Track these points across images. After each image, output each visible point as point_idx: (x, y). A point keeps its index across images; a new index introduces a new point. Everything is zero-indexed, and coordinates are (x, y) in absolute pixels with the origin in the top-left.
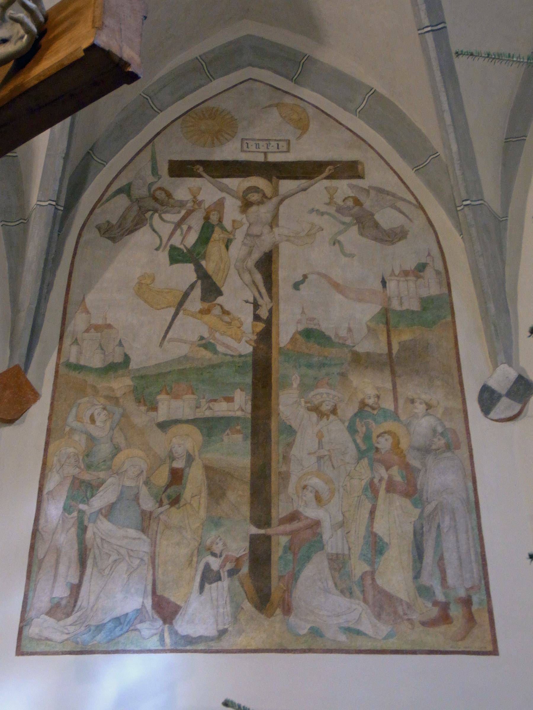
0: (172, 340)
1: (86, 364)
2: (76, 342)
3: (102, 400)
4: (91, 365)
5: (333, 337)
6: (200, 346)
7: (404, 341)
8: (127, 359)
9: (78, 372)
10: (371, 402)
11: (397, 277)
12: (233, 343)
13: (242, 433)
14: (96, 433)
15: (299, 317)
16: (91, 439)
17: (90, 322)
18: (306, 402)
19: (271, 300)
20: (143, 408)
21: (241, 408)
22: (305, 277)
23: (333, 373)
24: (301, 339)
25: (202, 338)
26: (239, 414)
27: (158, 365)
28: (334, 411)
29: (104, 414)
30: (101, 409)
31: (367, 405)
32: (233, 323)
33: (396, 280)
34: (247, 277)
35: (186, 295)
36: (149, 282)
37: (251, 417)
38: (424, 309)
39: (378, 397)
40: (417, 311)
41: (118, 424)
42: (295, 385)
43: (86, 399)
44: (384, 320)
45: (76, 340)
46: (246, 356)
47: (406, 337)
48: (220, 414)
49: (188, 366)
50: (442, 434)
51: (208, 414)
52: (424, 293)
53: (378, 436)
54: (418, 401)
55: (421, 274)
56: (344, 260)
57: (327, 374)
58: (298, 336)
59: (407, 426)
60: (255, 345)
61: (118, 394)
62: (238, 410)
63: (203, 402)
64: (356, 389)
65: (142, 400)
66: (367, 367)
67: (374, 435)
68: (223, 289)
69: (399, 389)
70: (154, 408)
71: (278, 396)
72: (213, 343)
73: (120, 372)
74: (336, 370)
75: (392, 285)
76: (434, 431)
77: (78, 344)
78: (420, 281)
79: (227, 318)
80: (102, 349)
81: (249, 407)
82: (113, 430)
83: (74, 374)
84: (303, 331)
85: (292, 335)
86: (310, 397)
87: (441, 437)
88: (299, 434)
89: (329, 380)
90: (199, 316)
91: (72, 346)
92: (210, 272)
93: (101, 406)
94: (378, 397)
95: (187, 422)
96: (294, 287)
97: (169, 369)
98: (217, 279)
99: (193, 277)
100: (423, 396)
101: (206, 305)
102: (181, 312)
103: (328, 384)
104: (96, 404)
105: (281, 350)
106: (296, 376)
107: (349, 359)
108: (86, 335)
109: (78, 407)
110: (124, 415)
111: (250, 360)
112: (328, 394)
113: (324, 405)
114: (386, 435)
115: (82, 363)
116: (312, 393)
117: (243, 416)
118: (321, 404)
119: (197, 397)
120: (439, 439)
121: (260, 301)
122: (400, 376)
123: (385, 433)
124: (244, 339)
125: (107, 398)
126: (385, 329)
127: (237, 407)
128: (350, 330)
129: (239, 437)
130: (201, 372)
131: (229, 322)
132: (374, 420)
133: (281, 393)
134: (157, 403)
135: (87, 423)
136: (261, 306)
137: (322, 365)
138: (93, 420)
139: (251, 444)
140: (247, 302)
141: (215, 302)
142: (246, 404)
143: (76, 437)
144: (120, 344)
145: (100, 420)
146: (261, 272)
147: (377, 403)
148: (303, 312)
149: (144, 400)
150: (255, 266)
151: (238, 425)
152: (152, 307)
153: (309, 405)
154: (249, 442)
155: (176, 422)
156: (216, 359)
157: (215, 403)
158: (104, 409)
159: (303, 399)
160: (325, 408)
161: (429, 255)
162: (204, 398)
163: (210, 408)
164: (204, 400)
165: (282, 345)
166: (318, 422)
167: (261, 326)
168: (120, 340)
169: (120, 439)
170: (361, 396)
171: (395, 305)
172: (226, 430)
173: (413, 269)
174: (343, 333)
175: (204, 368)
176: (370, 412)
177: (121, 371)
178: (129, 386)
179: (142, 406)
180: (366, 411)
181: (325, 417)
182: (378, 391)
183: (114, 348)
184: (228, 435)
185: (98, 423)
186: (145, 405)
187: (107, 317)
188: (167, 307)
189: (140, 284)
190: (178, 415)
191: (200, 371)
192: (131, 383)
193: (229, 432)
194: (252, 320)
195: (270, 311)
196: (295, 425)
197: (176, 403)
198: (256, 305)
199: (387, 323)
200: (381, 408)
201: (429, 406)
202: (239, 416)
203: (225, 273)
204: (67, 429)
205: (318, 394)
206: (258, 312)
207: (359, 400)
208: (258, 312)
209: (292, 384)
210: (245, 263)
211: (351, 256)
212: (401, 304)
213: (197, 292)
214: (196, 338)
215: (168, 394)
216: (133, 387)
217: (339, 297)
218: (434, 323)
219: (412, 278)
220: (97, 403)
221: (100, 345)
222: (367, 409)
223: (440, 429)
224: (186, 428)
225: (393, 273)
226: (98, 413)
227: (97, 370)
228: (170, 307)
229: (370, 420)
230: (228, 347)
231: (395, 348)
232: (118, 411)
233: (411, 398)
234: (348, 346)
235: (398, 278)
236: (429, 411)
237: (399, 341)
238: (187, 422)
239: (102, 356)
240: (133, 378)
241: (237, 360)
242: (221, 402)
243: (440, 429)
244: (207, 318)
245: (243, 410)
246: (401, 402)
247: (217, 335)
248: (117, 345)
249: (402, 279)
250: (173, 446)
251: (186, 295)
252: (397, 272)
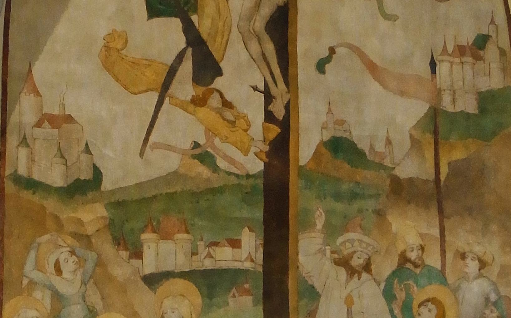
0: (157, 146)
1: (42, 180)
2: (24, 142)
3: (70, 240)
4: (49, 182)
5: (367, 153)
6: (194, 157)
7: (456, 161)
8: (97, 174)
9: (31, 191)
10: (413, 255)
11: (450, 56)
12: (238, 156)
13: (252, 295)
14: (64, 288)
15: (324, 118)
16: (57, 296)
17: (41, 110)
18: (332, 252)
19: (288, 87)
20: (124, 254)
21: (251, 258)
22: (332, 50)
23: (367, 210)
24: (327, 154)
25: (196, 145)
26: (248, 265)
27: (139, 185)
28: (367, 267)
29: (73, 260)
30: (68, 253)
31: (409, 261)
32: (237, 122)
33: (449, 61)
34: (254, 47)
35: (172, 72)
36: (119, 46)
37: (263, 271)
38: (483, 110)
39: (422, 248)
40: (474, 114)
41: (91, 277)
42: (319, 226)
43: (47, 237)
44: (432, 128)
45: (25, 138)
46: (254, 176)
47: (458, 155)
48: (224, 265)
49: (178, 188)
50: (495, 304)
51: (208, 264)
52: (484, 84)
53: (419, 306)
54: (470, 255)
55: (481, 53)
56: (384, 24)
57: (360, 211)
58: (324, 150)
59: (455, 291)
60: (267, 160)
61: (90, 230)
62: (246, 260)
63: (201, 244)
64: (396, 234)
65: (122, 242)
66: (409, 202)
67: (415, 304)
68: (222, 65)
69: (448, 238)
70: (138, 254)
71: (297, 241)
72: (211, 154)
73: (90, 195)
74: (370, 205)
75: (443, 69)
76: (487, 299)
77: (28, 146)
78: (480, 63)
79: (229, 115)
80: (62, 157)
81: (259, 257)
82: (85, 285)
83: (27, 195)
84: (329, 141)
85: (315, 147)
86: (338, 244)
87: (493, 308)
88: (322, 299)
89: (362, 220)
90: (191, 107)
91: (20, 149)
92: (205, 36)
93: (68, 249)
94: (422, 248)
95: (183, 275)
96: (317, 68)
97: (154, 192)
98: (214, 48)
99: (181, 41)
100: (477, 249)
101: (201, 90)
102: (167, 100)
103: (360, 226)
104: (61, 244)
105: (300, 168)
106: (320, 213)
107: (387, 188)
108: (37, 130)
109: (38, 249)
110: (100, 263)
111: (260, 182)
112: (361, 241)
113: (355, 257)
114: (430, 303)
115: (36, 177)
116: (340, 240)
117: (252, 269)
118: (351, 255)
119: (192, 238)
120: (492, 311)
121: (274, 91)
122: (449, 218)
123: (428, 300)
124: (253, 149)
125: (76, 236)
126: (432, 141)
127: (244, 256)
128: (389, 142)
129: (248, 300)
130: (197, 199)
131: (234, 122)
132: (416, 282)
133: (300, 237)
134: (142, 246)
135: (51, 273)
136: (274, 97)
137: (354, 196)
138: (58, 271)
139: (264, 310)
140: (255, 89)
141: (212, 86)
142: (256, 252)
143: (38, 294)
144: (87, 150)
145: (68, 267)
146: (272, 39)
147: (421, 258)
148: (330, 111)
149: (125, 241)
150: (266, 30)
151: (247, 283)
152: (127, 90)
153: (336, 256)
154: (261, 308)
155: (168, 275)
156: (217, 181)
157: (217, 248)
158: (72, 253)
159: (329, 247)
160: (357, 262)
161: (492, 22)
162: (202, 240)
163: (209, 256)
164: (202, 243)
165: (302, 162)
166: (347, 282)
167: (275, 131)
168: (87, 144)
169: (95, 299)
170: (401, 247)
171: (447, 104)
172: (232, 288)
173: (470, 44)
174: (380, 147)
175: (201, 192)
176: (411, 270)
177: (91, 193)
178: (103, 217)
179: (123, 250)
180: (407, 268)
181: (356, 275)
182: (422, 239)
183: (79, 156)
184: (234, 296)
185: (66, 274)
186: (126, 249)
187: (64, 103)
188: (146, 91)
189: (107, 48)
190: (169, 267)
191: (195, 195)
192: (105, 213)
193: (236, 292)
194: (263, 121)
195: (287, 107)
196: (318, 287)
197: (167, 246)
198: (269, 98)
199: (436, 133)
200: (425, 266)
201: (483, 264)
202: (248, 268)
203: (226, 38)
204: (25, 282)
205: (348, 241)
206: (270, 108)
207: (399, 252)
208: (270, 108)
209: (315, 225)
210: (252, 23)
211: (390, 18)
212: (454, 101)
213: (187, 67)
214: (188, 145)
215: (154, 232)
216: (108, 220)
217: (375, 87)
218: (494, 134)
219: (468, 59)
220: (62, 243)
221: (59, 149)
222: (409, 265)
223: (493, 297)
224: (180, 284)
225: (445, 51)
226: (65, 260)
227: (59, 190)
228: (151, 90)
229: (411, 282)
230: (232, 161)
231: (444, 170)
232: (91, 256)
233: (461, 250)
234: (385, 168)
235: (451, 59)
236: (482, 271)
237: (450, 161)
238: (183, 275)
239: (64, 167)
240: (108, 206)
241: (243, 182)
242: (224, 246)
243: (493, 297)
244: (202, 112)
245: (252, 261)
246: (449, 255)
247: (217, 141)
248: (82, 152)
249: (457, 60)
250: (165, 312)
251: (172, 72)
252: (450, 49)
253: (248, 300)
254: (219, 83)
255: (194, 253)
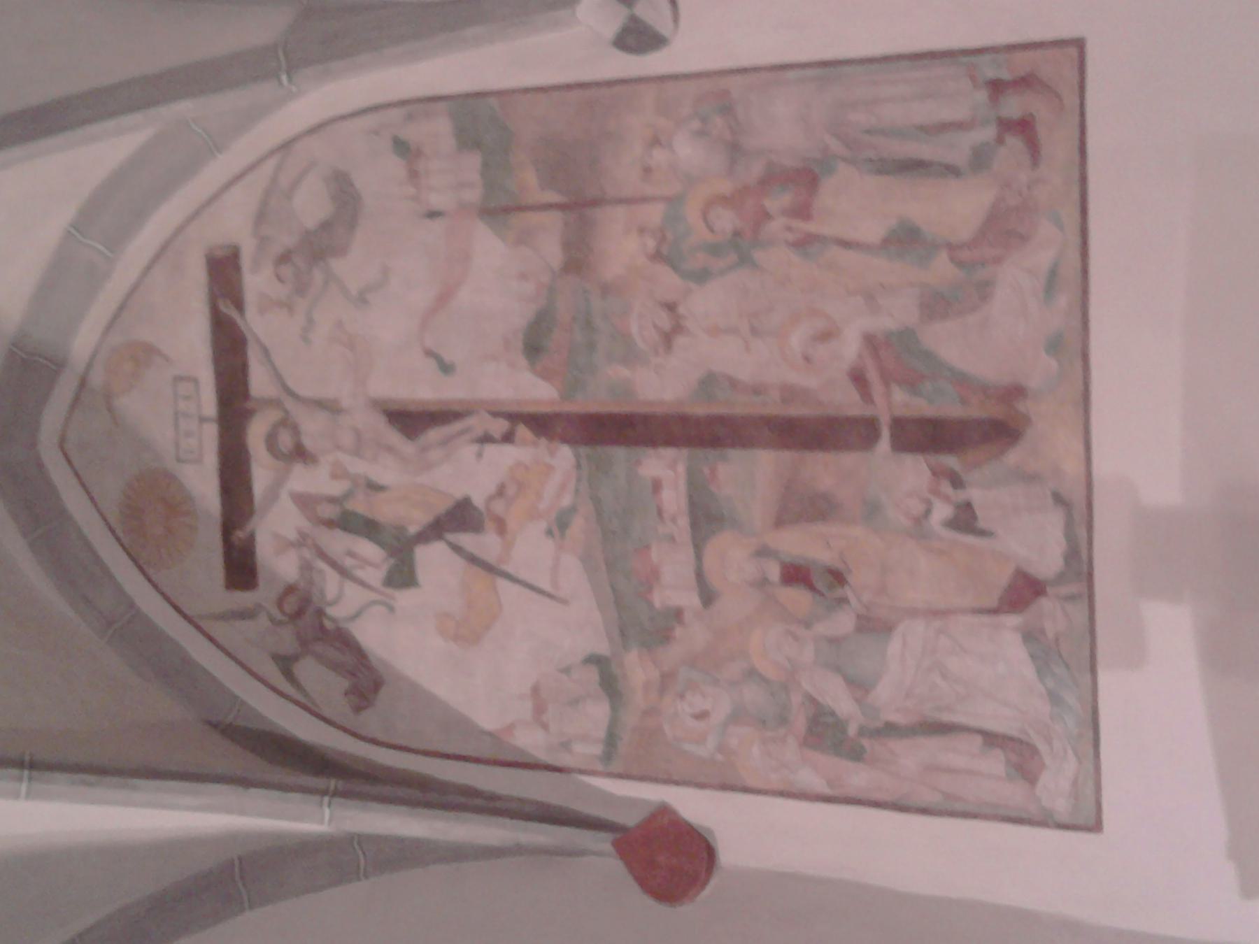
8: (595, 660)
10: (651, 244)
20: (678, 632)
25: (549, 533)
26: (681, 468)
28: (671, 307)
34: (434, 455)
35: (473, 560)
38: (477, 145)
42: (624, 372)
43: (666, 727)
47: (530, 177)
48: (684, 502)
50: (704, 120)
51: (684, 522)
75: (437, 200)
79: (511, 490)
95: (699, 557)
98: (442, 507)
101: (489, 525)
115: (601, 733)
121: (479, 432)
123: (705, 219)
129: (723, 470)
137: (588, 325)
138: (702, 716)
144: (566, 670)
155: (700, 575)
158: (682, 696)
160: (665, 321)
163: (674, 520)
167: (523, 431)
190: (689, 572)
195: (496, 414)
198: (486, 439)
199: (507, 210)
201: (655, 142)
204: (719, 757)
213: (466, 540)
223: (696, 125)
227: (614, 709)
231: (551, 197)
238: (699, 557)
247: (542, 506)
251: (473, 560)
253: (723, 470)
254: (478, 500)
255: (672, 539)
